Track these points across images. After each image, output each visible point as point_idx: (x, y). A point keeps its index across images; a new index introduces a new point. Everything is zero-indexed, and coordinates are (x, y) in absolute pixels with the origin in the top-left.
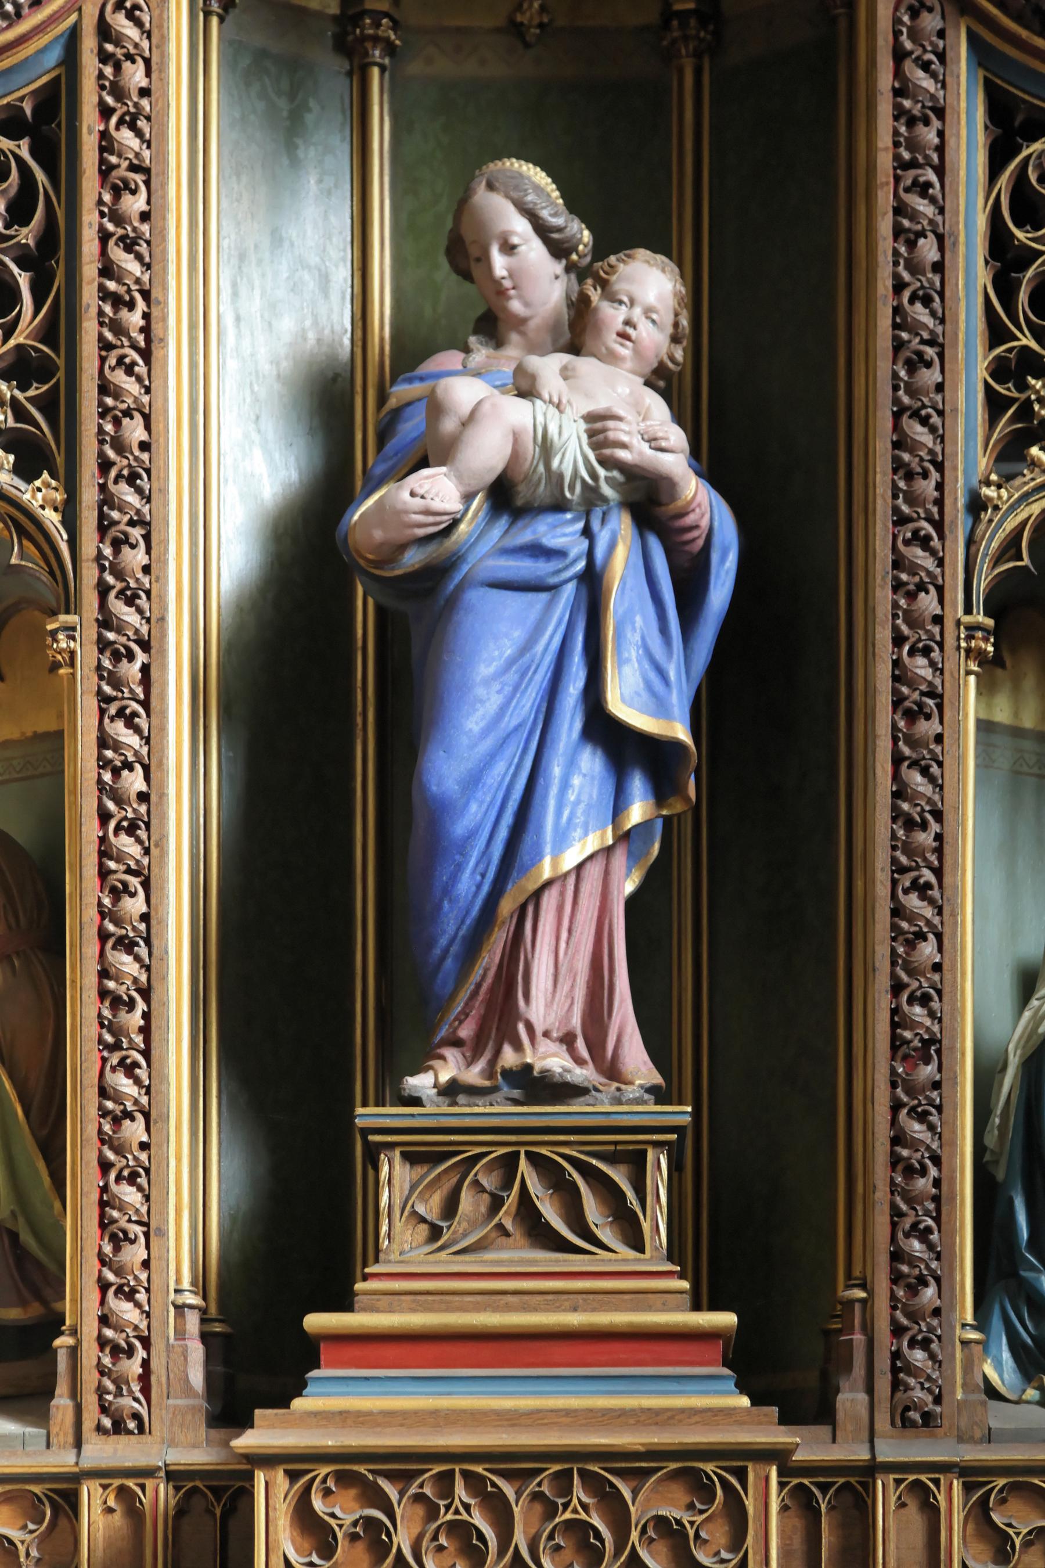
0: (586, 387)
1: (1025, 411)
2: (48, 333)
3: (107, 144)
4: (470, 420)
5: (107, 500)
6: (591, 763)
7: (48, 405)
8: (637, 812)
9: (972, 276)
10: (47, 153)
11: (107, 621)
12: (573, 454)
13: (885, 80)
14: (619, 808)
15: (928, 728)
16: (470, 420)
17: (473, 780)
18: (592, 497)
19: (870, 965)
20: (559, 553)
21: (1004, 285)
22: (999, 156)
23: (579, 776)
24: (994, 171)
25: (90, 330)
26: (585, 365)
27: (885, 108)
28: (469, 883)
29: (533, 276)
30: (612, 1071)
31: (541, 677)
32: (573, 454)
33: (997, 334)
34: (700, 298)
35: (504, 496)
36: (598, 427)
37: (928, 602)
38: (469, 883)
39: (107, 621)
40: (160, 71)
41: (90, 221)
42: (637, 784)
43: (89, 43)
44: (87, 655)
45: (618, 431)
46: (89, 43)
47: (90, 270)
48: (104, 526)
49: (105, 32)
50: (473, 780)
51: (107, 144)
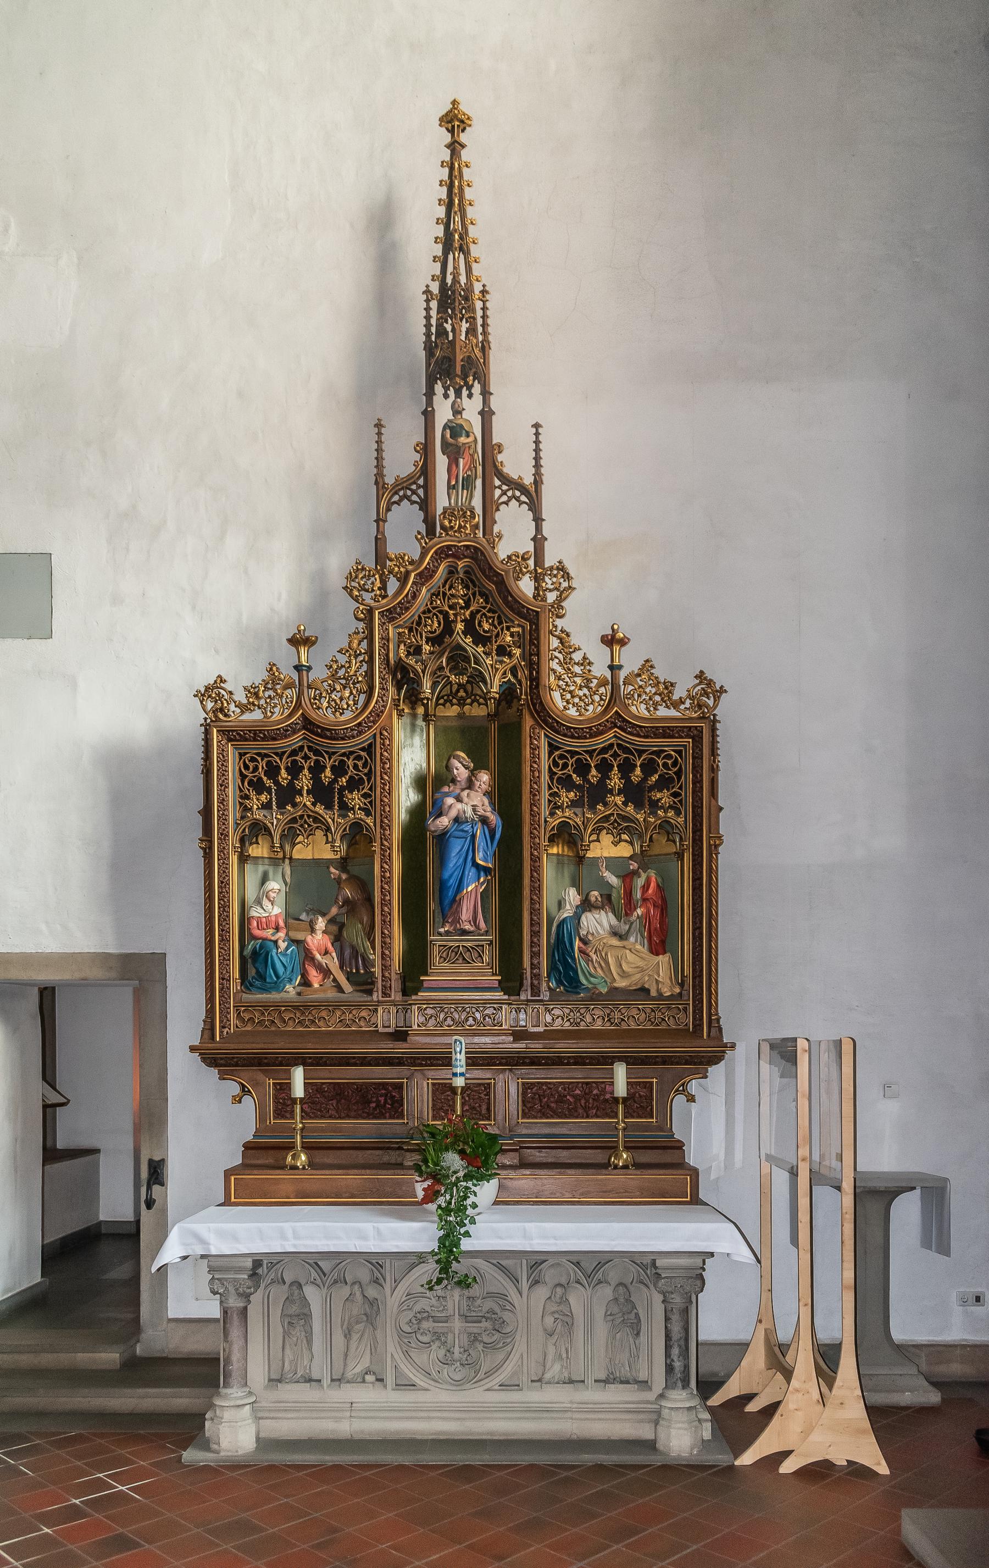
0: (471, 802)
1: (555, 803)
2: (370, 789)
3: (382, 755)
4: (450, 807)
5: (382, 821)
6: (473, 870)
7: (370, 802)
8: (482, 880)
9: (545, 778)
10: (370, 754)
11: (382, 844)
12: (469, 812)
13: (528, 742)
14: (479, 879)
15: (537, 864)
16: (450, 807)
17: (451, 876)
18: (473, 820)
19: (280, 1415)
20: (467, 831)
21: (551, 778)
22: (550, 754)
23: (471, 873)
24: (549, 758)
25: (378, 789)
26: (473, 793)
27: (528, 747)
28: (451, 893)
29: (461, 772)
30: (478, 927)
31: (464, 855)
32: (469, 812)
33: (550, 788)
34: (493, 778)
35: (457, 820)
36: (474, 808)
37: (537, 840)
38: (451, 893)
39: (382, 844)
40: (644, 1192)
41: (378, 768)
42: (482, 873)
43: (378, 736)
44: (378, 849)
45: (478, 809)
46: (378, 736)
47: (378, 778)
48: (381, 826)
49: (381, 734)
50: (451, 876)
51: (382, 755)
